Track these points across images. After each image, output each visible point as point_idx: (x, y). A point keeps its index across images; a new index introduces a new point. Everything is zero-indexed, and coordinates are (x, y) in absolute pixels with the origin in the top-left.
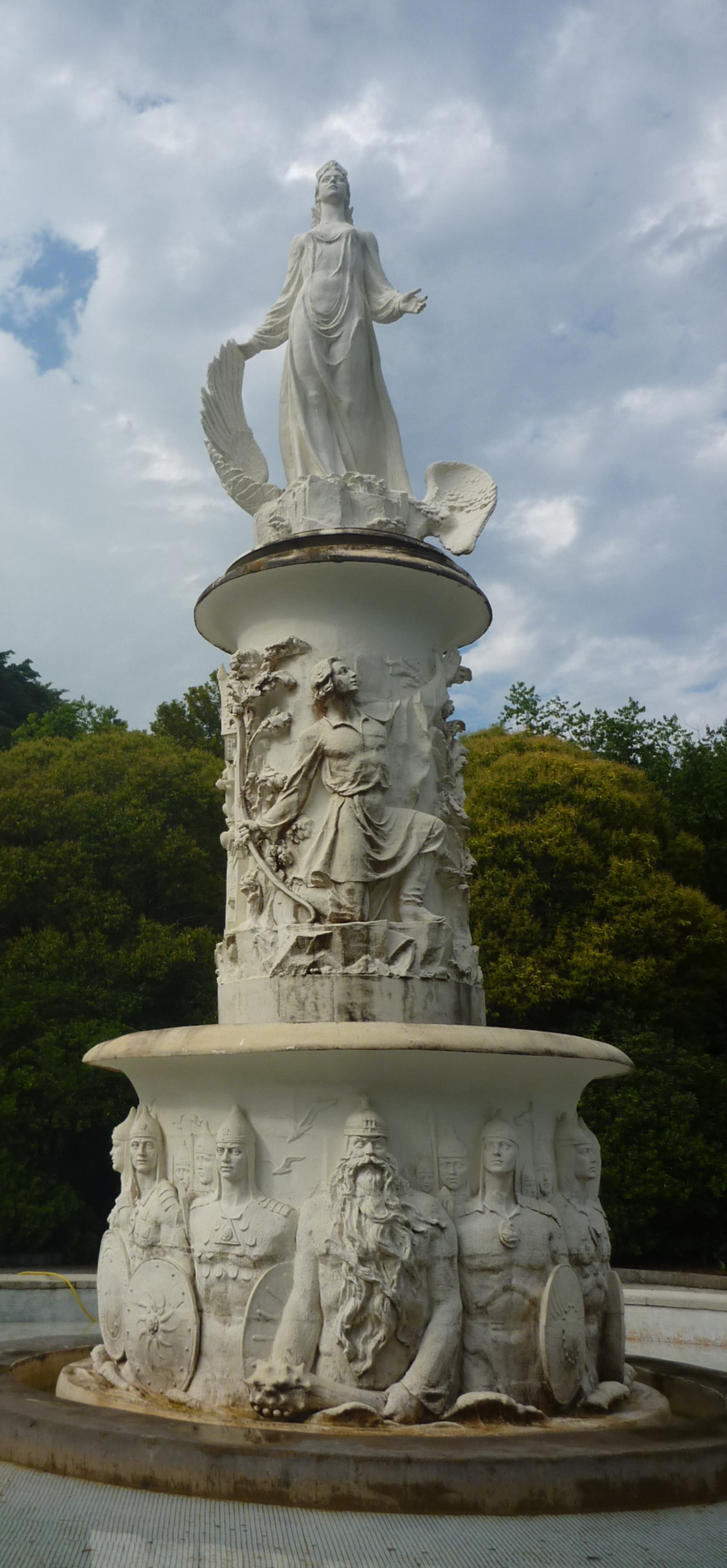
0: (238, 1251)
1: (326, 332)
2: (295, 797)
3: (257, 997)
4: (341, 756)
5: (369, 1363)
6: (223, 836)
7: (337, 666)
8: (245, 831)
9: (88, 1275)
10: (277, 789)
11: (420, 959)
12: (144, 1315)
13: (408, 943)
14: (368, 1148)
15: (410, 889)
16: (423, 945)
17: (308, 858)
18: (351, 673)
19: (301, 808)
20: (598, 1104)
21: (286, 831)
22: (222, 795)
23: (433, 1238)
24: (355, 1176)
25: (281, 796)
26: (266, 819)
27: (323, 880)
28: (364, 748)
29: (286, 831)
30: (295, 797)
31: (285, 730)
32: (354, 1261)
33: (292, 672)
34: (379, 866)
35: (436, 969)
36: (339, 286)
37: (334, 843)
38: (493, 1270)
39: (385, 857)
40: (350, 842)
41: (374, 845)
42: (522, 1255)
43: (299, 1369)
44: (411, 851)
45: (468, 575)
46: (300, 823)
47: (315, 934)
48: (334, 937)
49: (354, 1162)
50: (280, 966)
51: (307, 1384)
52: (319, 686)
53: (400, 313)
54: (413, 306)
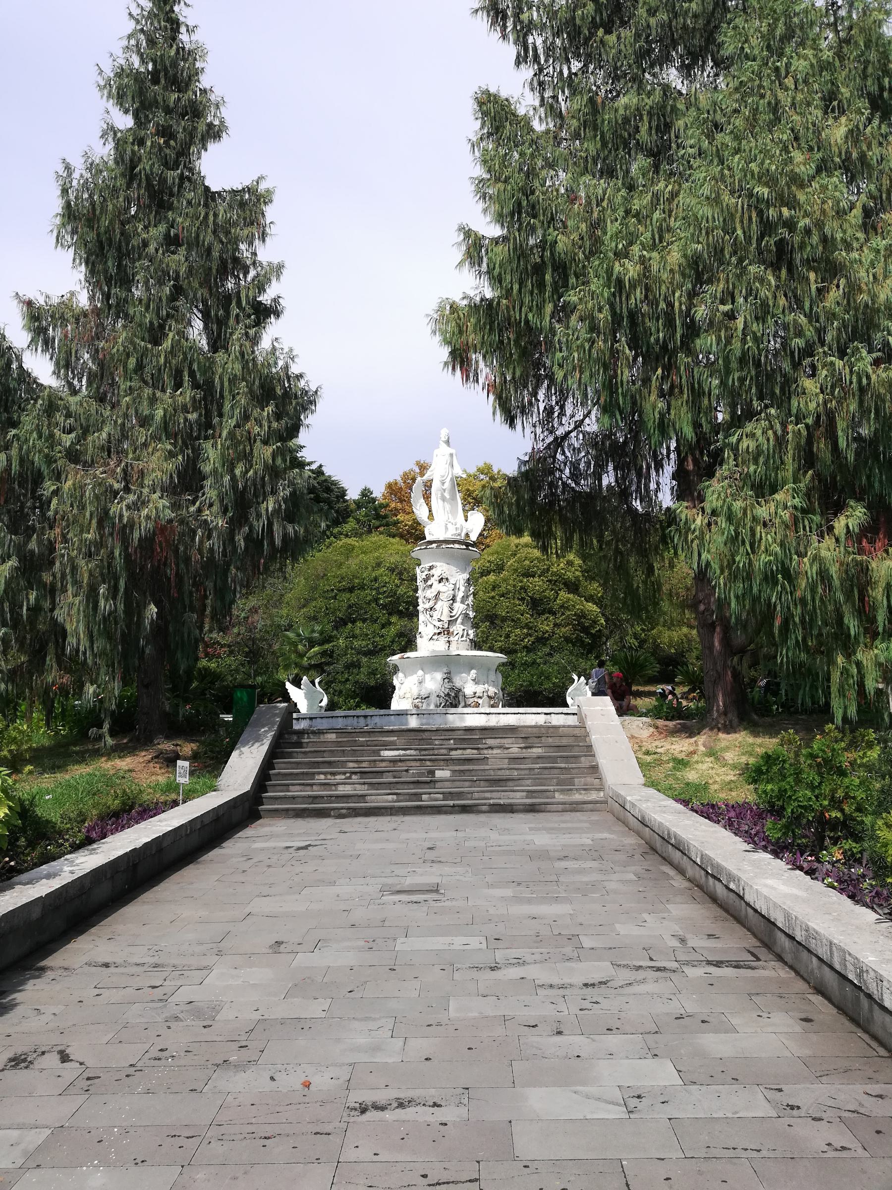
15: (459, 620)
17: (436, 615)
27: (440, 620)
31: (431, 586)
33: (433, 572)
40: (446, 610)
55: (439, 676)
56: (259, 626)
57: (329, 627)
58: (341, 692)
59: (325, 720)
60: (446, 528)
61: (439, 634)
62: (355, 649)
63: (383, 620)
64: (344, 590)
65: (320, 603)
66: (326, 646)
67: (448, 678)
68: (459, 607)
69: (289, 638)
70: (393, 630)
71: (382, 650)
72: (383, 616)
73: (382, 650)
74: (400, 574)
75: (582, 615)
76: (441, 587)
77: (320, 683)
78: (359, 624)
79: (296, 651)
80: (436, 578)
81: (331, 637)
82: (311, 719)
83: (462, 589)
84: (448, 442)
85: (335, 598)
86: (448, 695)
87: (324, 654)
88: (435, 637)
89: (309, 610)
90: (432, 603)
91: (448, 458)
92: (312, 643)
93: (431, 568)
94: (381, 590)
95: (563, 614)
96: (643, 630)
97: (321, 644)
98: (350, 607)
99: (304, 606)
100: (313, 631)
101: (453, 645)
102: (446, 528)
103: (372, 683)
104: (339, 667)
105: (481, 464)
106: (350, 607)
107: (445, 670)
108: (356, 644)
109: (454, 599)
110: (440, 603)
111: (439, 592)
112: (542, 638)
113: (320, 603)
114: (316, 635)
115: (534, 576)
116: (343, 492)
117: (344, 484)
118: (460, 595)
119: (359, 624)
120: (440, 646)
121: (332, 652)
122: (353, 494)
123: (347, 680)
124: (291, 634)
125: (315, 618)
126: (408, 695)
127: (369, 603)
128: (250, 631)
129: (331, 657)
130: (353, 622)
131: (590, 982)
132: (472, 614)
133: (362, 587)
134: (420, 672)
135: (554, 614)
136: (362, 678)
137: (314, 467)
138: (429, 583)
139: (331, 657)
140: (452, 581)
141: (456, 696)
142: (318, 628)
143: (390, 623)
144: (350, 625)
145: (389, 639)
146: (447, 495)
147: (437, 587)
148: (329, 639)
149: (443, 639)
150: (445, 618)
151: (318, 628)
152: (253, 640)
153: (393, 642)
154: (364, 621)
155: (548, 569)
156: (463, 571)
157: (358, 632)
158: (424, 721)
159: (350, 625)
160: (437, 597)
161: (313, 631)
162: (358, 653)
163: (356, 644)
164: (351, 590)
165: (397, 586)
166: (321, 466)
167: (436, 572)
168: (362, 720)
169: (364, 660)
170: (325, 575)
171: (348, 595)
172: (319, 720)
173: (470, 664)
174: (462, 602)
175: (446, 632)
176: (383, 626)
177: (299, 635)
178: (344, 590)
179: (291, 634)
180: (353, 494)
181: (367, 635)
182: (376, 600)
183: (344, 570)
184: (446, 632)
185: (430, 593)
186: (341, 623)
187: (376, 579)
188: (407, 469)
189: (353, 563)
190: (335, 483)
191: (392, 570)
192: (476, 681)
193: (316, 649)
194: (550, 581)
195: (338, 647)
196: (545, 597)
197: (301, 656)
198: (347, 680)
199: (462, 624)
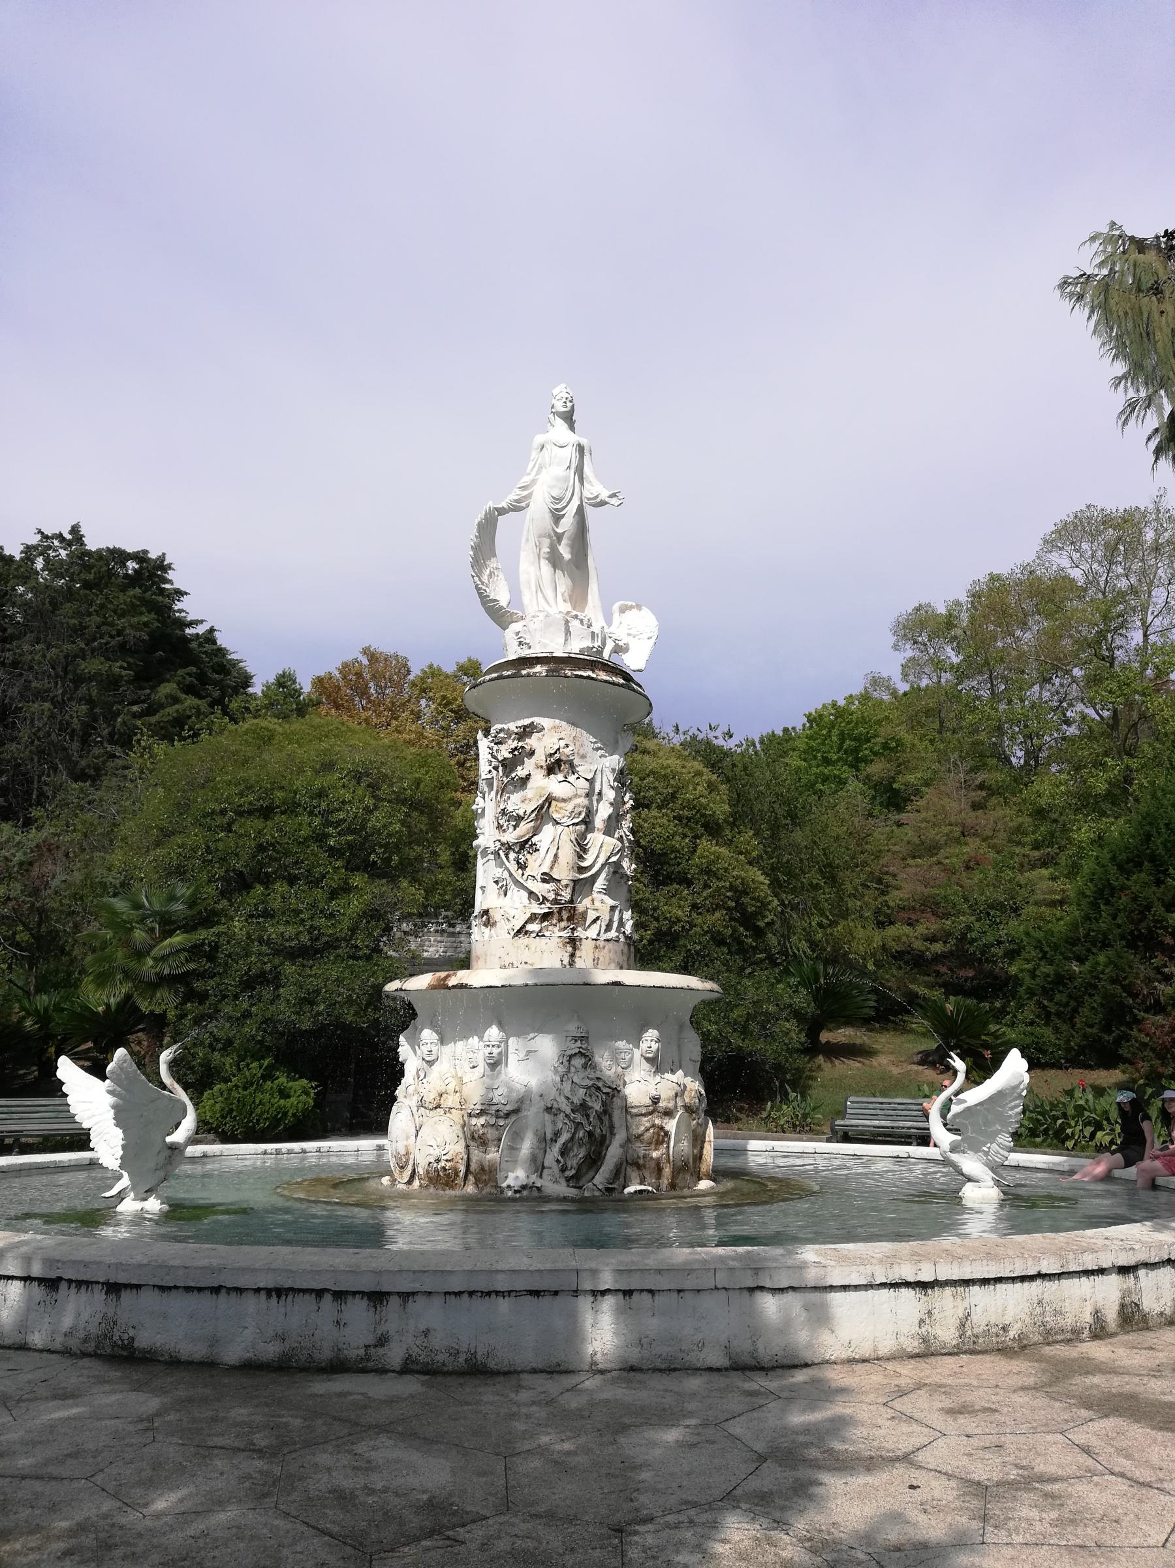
0: (495, 1108)
1: (556, 510)
2: (532, 824)
3: (505, 948)
4: (564, 800)
5: (573, 1172)
6: (475, 843)
7: (562, 743)
8: (498, 844)
9: (9, 1157)
10: (519, 819)
11: (604, 928)
12: (431, 1151)
13: (598, 918)
14: (579, 1044)
15: (600, 883)
16: (606, 917)
17: (537, 864)
18: (571, 748)
19: (536, 831)
20: (702, 1014)
21: (525, 845)
22: (476, 816)
23: (613, 1096)
24: (569, 1061)
25: (523, 823)
26: (511, 836)
27: (547, 878)
28: (576, 796)
29: (525, 845)
30: (532, 824)
31: (525, 781)
32: (568, 1111)
33: (532, 742)
34: (581, 870)
35: (613, 934)
36: (567, 479)
37: (556, 855)
38: (644, 1115)
39: (585, 864)
40: (567, 853)
41: (580, 857)
42: (662, 1104)
43: (534, 1176)
44: (601, 860)
45: (640, 686)
46: (534, 840)
47: (542, 912)
48: (1098, 1082)
49: (569, 1052)
50: (519, 931)
51: (539, 1185)
52: (551, 755)
53: (603, 503)
54: (614, 501)
55: (547, 1046)
56: (54, 883)
57: (210, 891)
58: (229, 1042)
59: (177, 1303)
60: (568, 632)
61: (545, 917)
62: (268, 943)
63: (334, 882)
64: (250, 813)
65: (195, 837)
66: (203, 934)
67: (580, 1056)
68: (602, 846)
69: (114, 913)
70: (355, 904)
71: (329, 946)
72: (334, 871)
73: (329, 946)
74: (373, 787)
75: (741, 891)
76: (555, 785)
77: (173, 1065)
78: (281, 887)
79: (127, 943)
80: (540, 757)
81: (214, 913)
82: (114, 1288)
83: (610, 795)
84: (569, 418)
85: (228, 828)
86: (583, 1107)
87: (195, 951)
88: (534, 927)
89: (170, 852)
90: (524, 828)
91: (570, 453)
92: (168, 926)
93: (526, 732)
94: (333, 818)
95: (706, 886)
96: (820, 925)
97: (188, 928)
98: (261, 848)
99: (158, 844)
100: (172, 898)
101: (584, 961)
102: (568, 632)
103: (306, 1024)
104: (231, 982)
105: (463, 660)
106: (261, 848)
107: (572, 1028)
108: (273, 931)
109: (588, 822)
110: (548, 831)
111: (549, 800)
112: (669, 932)
113: (195, 837)
114: (178, 907)
115: (648, 807)
116: (246, 680)
117: (250, 667)
118: (604, 811)
119: (281, 887)
120: (546, 953)
121: (215, 947)
122: (261, 681)
123: (247, 1015)
124: (120, 905)
125: (180, 872)
126: (451, 1101)
127: (303, 843)
128: (35, 892)
129: (211, 958)
130: (267, 881)
131: (477, 1301)
132: (628, 866)
133: (292, 808)
134: (494, 1033)
135: (688, 883)
136: (284, 1011)
137: (201, 630)
138: (521, 772)
139: (211, 958)
140: (584, 770)
141: (606, 1112)
142: (183, 890)
143: (346, 889)
144: (259, 889)
145: (346, 923)
146: (565, 551)
147: (542, 784)
148: (208, 919)
149: (556, 933)
150: (564, 873)
151: (183, 890)
152: (43, 913)
153: (353, 930)
154: (292, 880)
155: (673, 796)
156: (611, 747)
157: (276, 904)
158: (653, 1325)
159: (259, 889)
160: (543, 813)
161: (172, 898)
162: (277, 952)
163: (273, 931)
164: (266, 813)
165: (366, 808)
166: (212, 630)
167: (543, 744)
168: (357, 1310)
169: (289, 969)
170: (208, 781)
171: (259, 823)
172: (148, 1299)
173: (636, 1011)
174: (608, 832)
175: (563, 913)
176: (334, 894)
177: (138, 906)
178: (250, 813)
179: (120, 905)
180: (261, 681)
181: (297, 912)
182: (320, 838)
183: (250, 773)
184: (563, 913)
185: (522, 802)
186: (239, 884)
187: (321, 794)
188: (349, 657)
189: (273, 759)
190: (235, 664)
191: (358, 777)
192: (658, 1064)
193: (178, 939)
194: (679, 818)
195: (230, 937)
196: (674, 850)
197: (140, 954)
198: (247, 1015)
199: (608, 891)
